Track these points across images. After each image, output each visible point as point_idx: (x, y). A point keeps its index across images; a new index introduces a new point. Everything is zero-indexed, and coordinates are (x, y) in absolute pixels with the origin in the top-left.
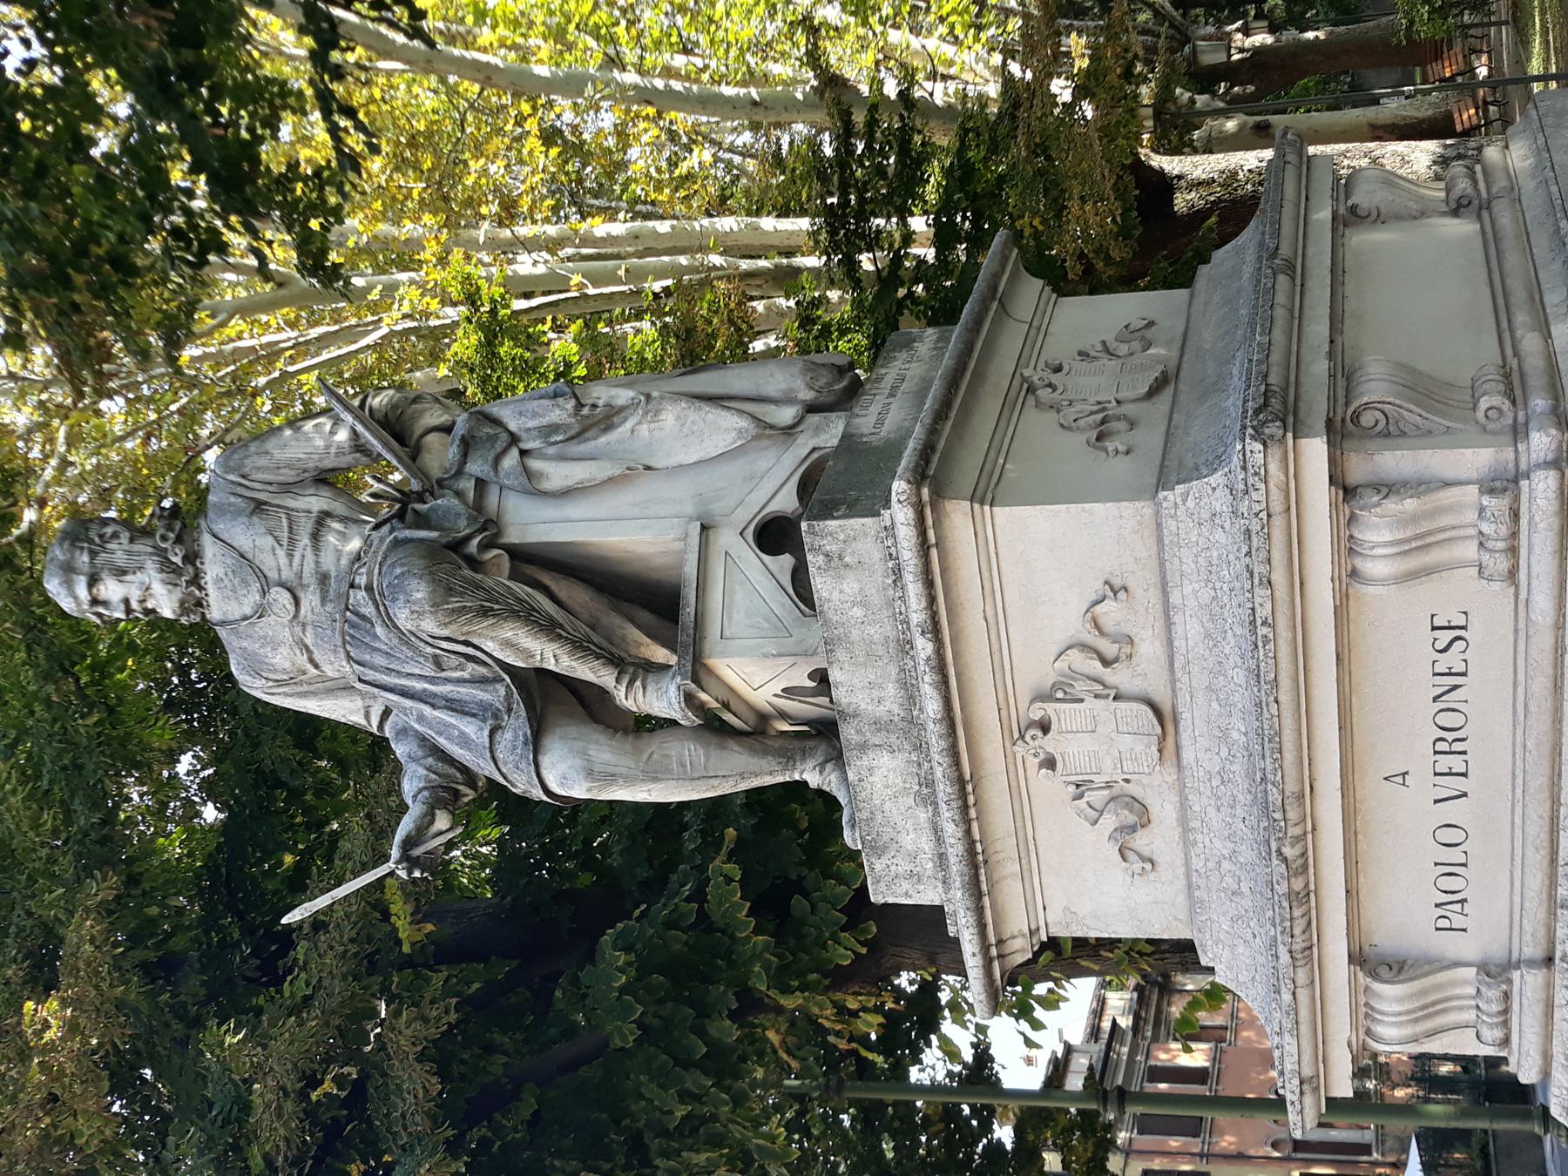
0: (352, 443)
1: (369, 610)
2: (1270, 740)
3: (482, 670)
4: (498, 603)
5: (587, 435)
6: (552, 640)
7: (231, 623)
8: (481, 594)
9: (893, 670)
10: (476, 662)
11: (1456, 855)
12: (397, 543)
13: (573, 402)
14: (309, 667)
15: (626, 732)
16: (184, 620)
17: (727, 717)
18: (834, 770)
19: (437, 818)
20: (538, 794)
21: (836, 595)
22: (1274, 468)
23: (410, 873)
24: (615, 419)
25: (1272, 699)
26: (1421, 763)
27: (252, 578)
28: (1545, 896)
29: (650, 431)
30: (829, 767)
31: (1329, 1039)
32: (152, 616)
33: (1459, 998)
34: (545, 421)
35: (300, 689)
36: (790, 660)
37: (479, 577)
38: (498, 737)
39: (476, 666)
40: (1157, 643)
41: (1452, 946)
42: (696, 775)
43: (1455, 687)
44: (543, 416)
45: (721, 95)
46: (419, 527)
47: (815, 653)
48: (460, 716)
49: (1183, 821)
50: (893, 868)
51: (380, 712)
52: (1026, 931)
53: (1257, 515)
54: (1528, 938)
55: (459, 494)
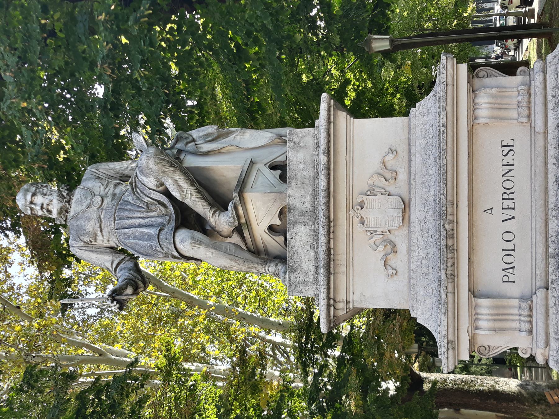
2: (443, 174)
9: (310, 190)
11: (510, 246)
21: (295, 159)
22: (449, 67)
25: (444, 157)
26: (497, 202)
28: (544, 256)
29: (240, 138)
31: (460, 328)
33: (512, 315)
35: (91, 249)
40: (405, 174)
41: (509, 289)
43: (510, 171)
45: (270, 320)
49: (409, 251)
50: (298, 279)
52: (345, 300)
53: (443, 83)
54: (538, 277)
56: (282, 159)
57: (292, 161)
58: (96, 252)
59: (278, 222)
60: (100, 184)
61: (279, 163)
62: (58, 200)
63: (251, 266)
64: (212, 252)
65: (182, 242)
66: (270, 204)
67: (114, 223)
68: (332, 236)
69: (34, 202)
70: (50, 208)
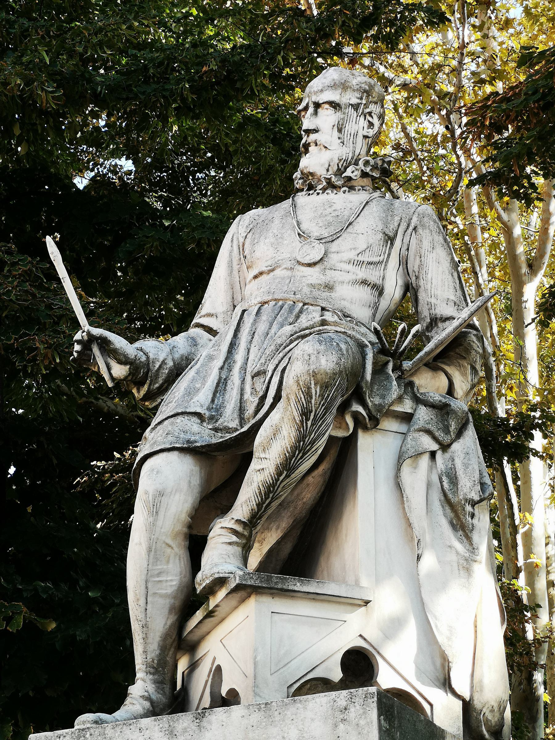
0: (439, 316)
1: (304, 321)
3: (250, 409)
4: (312, 425)
5: (447, 508)
6: (277, 468)
7: (295, 212)
8: (321, 411)
10: (258, 404)
12: (361, 346)
13: (477, 498)
14: (255, 272)
15: (190, 527)
16: (297, 175)
17: (199, 615)
18: (144, 709)
19: (123, 367)
20: (143, 449)
23: (79, 342)
24: (461, 532)
27: (332, 230)
30: (147, 704)
32: (302, 149)
34: (460, 473)
35: (235, 263)
36: (250, 672)
37: (334, 411)
38: (196, 420)
39: (255, 404)
42: (150, 585)
44: (465, 473)
46: (374, 364)
47: (256, 694)
48: (213, 389)
55: (400, 399)
57: (305, 708)
64: (140, 544)
69: (320, 110)
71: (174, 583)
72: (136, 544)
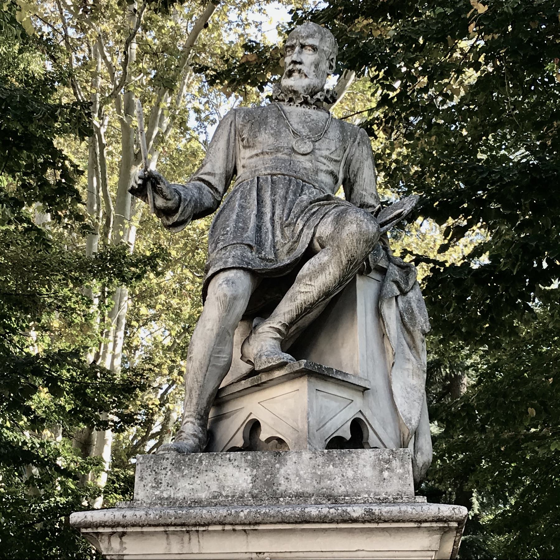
0: (366, 204)
4: (353, 268)
9: (310, 490)
35: (232, 140)
50: (164, 472)
51: (211, 181)
52: (125, 552)
56: (372, 439)
58: (228, 148)
59: (263, 436)
60: (334, 149)
61: (365, 435)
62: (309, 85)
63: (193, 392)
64: (212, 330)
65: (227, 281)
66: (290, 422)
67: (269, 174)
68: (228, 527)
70: (296, 74)
71: (226, 360)
72: (208, 330)
